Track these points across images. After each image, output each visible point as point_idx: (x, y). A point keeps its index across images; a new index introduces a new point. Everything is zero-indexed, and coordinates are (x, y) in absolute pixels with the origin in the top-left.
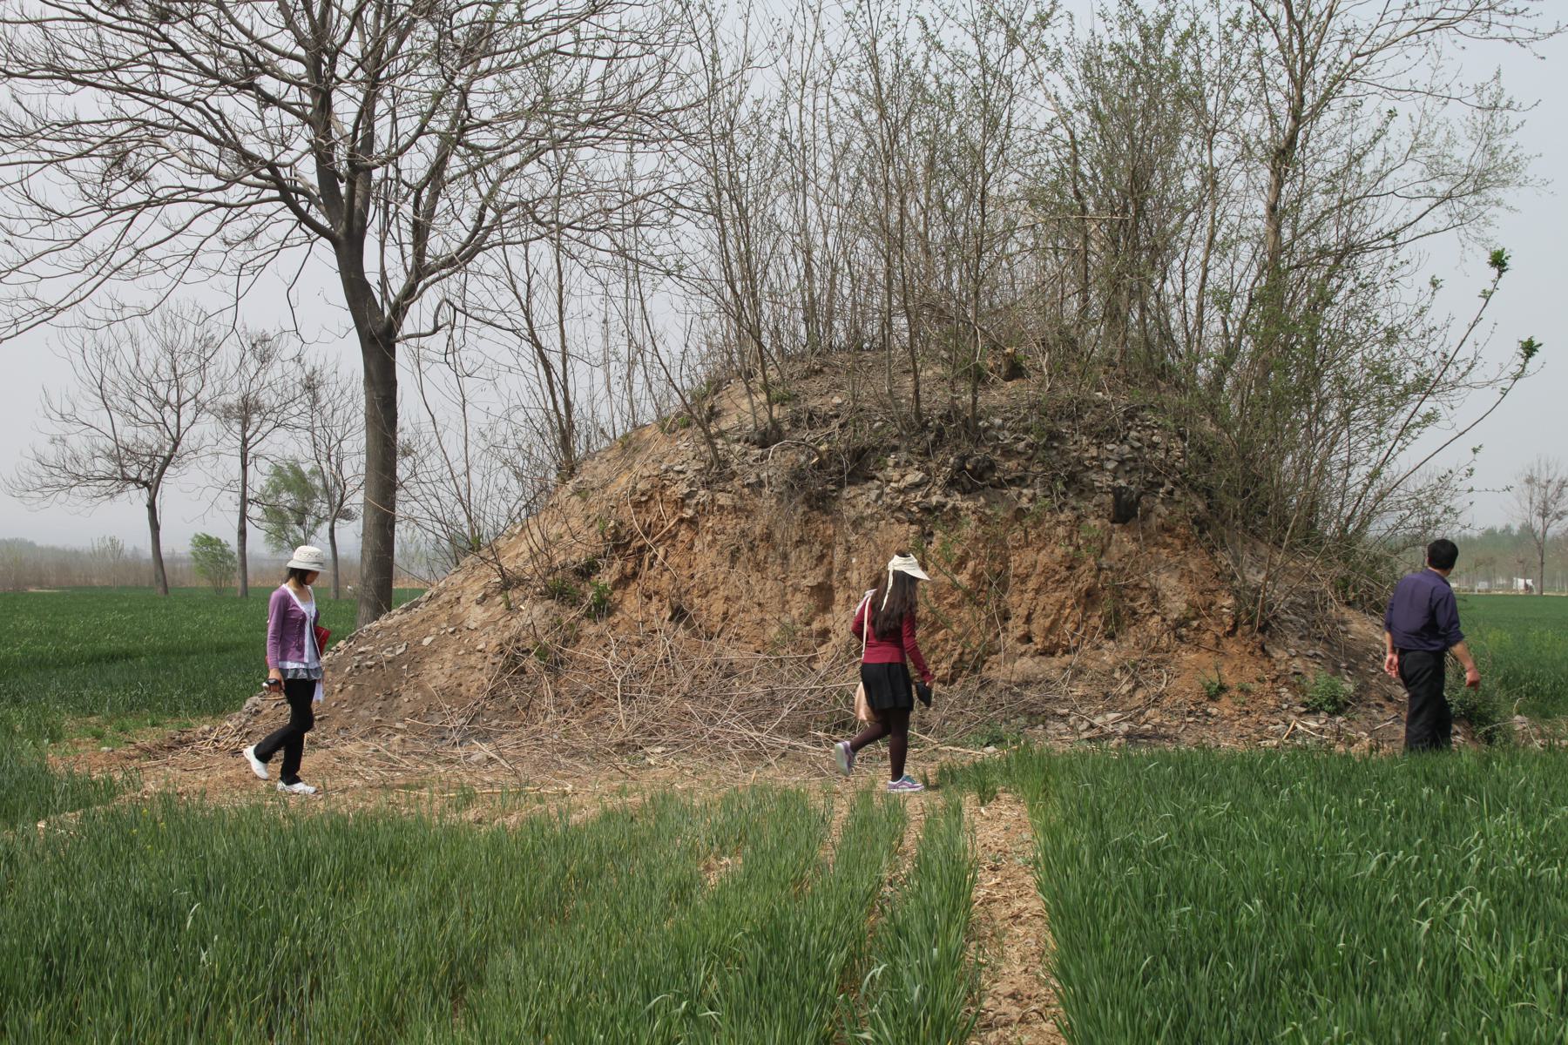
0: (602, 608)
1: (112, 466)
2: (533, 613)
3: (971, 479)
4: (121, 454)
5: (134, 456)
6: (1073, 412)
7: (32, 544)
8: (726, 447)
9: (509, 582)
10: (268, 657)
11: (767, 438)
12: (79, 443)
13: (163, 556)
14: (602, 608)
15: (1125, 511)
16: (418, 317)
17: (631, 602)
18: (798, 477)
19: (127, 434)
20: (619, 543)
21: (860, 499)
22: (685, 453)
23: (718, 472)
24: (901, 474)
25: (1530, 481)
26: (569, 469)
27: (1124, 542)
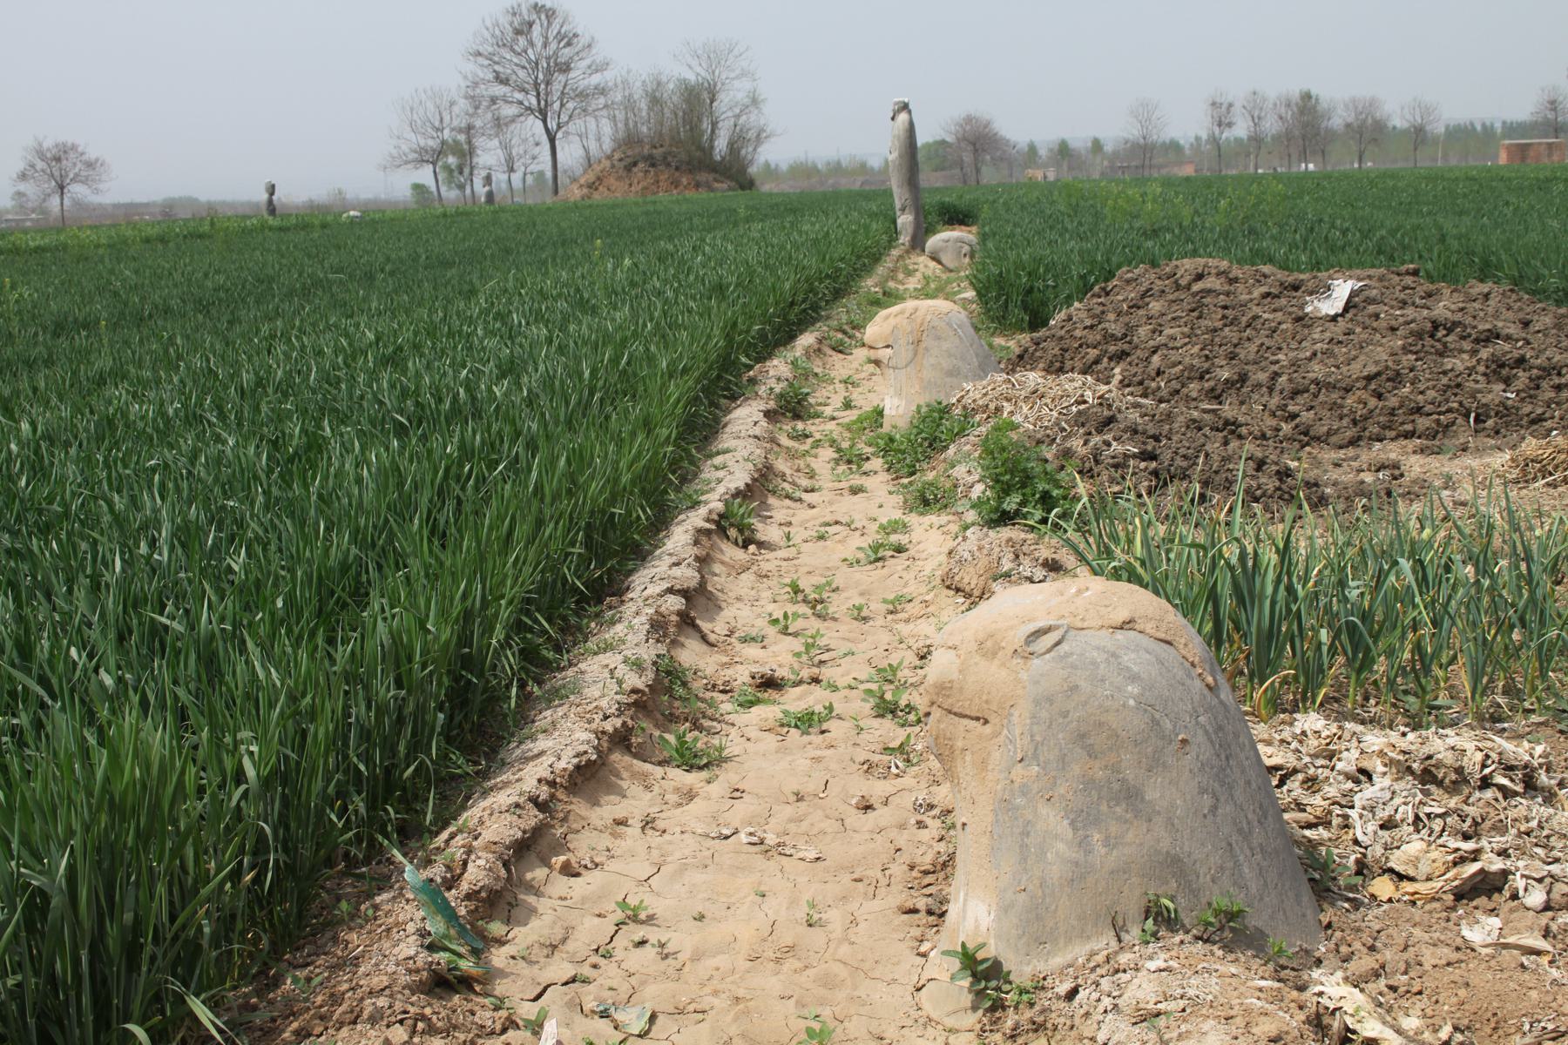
0: (596, 189)
1: (416, 155)
2: (585, 190)
3: (653, 165)
4: (422, 151)
5: (426, 151)
6: (670, 153)
7: (196, 200)
8: (97, 298)
9: (581, 186)
10: (91, 1018)
11: (621, 160)
12: (405, 148)
13: (920, 143)
14: (596, 189)
15: (677, 169)
16: (559, 135)
17: (601, 188)
18: (625, 167)
19: (422, 143)
20: (599, 179)
21: (635, 170)
22: (607, 164)
23: (613, 166)
24: (641, 165)
25: (1214, 104)
26: (590, 166)
27: (677, 174)
